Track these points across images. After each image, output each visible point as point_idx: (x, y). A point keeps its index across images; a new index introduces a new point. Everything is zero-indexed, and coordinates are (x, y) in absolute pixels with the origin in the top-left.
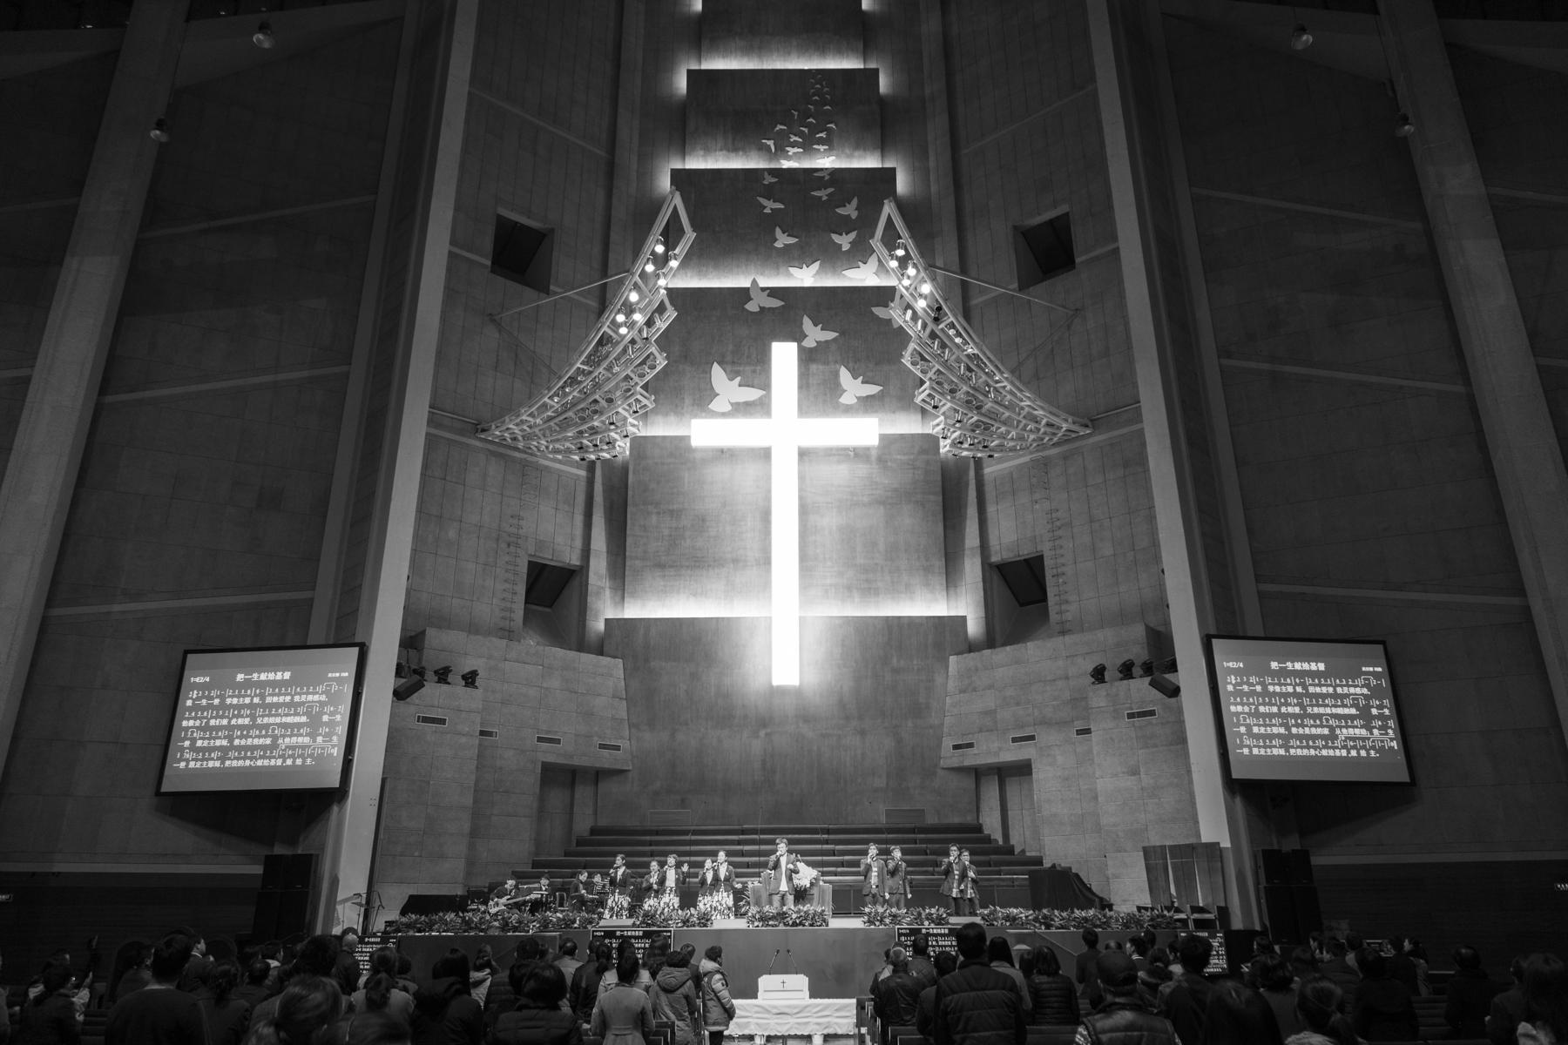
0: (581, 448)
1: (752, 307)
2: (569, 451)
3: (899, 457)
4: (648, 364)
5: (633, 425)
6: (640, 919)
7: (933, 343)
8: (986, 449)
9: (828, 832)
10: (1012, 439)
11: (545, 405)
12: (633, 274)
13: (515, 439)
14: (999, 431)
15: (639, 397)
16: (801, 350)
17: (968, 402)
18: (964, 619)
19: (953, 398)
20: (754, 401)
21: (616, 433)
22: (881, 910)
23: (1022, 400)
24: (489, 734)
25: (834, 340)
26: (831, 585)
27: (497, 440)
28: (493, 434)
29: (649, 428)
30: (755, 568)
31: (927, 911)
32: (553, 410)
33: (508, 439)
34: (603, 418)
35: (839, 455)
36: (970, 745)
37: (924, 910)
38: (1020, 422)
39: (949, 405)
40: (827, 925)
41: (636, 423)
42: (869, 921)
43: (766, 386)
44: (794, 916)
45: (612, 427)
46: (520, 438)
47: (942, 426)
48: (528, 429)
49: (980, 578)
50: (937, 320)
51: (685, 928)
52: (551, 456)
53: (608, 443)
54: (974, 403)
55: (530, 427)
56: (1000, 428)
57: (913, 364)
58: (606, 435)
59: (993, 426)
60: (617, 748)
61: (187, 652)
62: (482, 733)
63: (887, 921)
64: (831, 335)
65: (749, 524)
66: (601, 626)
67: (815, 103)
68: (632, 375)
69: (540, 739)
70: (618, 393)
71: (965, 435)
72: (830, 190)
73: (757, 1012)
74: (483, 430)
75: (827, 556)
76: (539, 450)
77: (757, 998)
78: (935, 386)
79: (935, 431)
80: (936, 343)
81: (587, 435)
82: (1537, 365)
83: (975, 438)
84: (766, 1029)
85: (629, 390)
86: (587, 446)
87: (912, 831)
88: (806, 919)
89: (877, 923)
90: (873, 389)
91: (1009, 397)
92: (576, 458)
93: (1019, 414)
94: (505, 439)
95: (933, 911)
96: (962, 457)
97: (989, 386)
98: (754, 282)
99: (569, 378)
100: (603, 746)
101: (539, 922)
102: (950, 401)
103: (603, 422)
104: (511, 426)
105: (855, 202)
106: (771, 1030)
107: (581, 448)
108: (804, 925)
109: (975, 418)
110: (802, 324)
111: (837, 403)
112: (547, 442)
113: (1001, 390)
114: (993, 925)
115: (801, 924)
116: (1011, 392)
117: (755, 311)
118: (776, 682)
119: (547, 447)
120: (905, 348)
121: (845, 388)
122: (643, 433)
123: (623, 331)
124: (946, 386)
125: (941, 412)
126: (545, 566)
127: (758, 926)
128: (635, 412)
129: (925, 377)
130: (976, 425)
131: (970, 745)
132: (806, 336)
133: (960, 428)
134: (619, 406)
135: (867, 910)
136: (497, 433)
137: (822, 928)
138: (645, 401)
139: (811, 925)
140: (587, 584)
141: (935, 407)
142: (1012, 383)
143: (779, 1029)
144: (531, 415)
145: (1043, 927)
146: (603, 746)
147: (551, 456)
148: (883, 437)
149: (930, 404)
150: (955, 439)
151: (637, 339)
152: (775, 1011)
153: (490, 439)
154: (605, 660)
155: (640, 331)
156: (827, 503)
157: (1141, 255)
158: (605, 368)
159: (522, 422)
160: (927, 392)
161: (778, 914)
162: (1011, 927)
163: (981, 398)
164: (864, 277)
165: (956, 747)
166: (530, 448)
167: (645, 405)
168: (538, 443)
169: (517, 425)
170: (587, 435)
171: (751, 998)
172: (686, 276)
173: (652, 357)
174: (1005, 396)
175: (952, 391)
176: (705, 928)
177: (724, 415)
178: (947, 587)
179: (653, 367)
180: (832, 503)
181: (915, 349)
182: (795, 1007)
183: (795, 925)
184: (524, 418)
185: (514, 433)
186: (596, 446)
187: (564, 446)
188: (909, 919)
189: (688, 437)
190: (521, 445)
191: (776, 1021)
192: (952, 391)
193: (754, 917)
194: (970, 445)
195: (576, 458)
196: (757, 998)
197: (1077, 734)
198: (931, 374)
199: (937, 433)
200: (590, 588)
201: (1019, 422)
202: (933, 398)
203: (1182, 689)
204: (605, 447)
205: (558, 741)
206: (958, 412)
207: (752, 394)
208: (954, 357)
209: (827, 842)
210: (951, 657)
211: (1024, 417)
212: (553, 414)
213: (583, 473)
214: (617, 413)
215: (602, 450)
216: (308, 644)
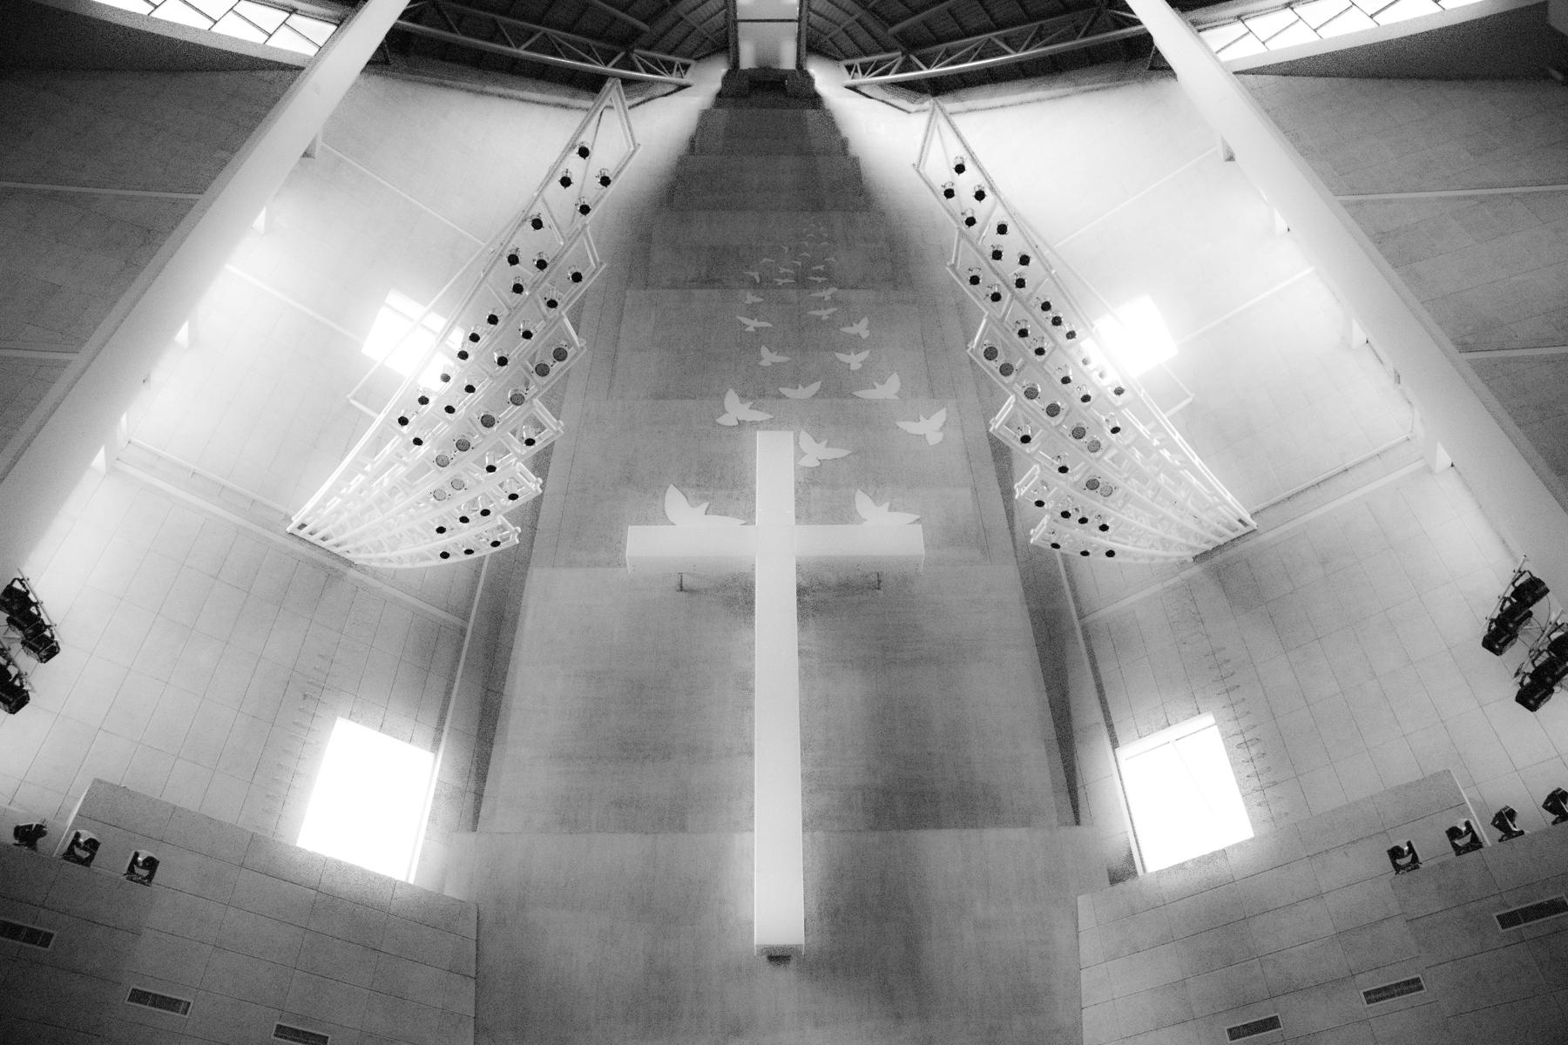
64: (840, 453)
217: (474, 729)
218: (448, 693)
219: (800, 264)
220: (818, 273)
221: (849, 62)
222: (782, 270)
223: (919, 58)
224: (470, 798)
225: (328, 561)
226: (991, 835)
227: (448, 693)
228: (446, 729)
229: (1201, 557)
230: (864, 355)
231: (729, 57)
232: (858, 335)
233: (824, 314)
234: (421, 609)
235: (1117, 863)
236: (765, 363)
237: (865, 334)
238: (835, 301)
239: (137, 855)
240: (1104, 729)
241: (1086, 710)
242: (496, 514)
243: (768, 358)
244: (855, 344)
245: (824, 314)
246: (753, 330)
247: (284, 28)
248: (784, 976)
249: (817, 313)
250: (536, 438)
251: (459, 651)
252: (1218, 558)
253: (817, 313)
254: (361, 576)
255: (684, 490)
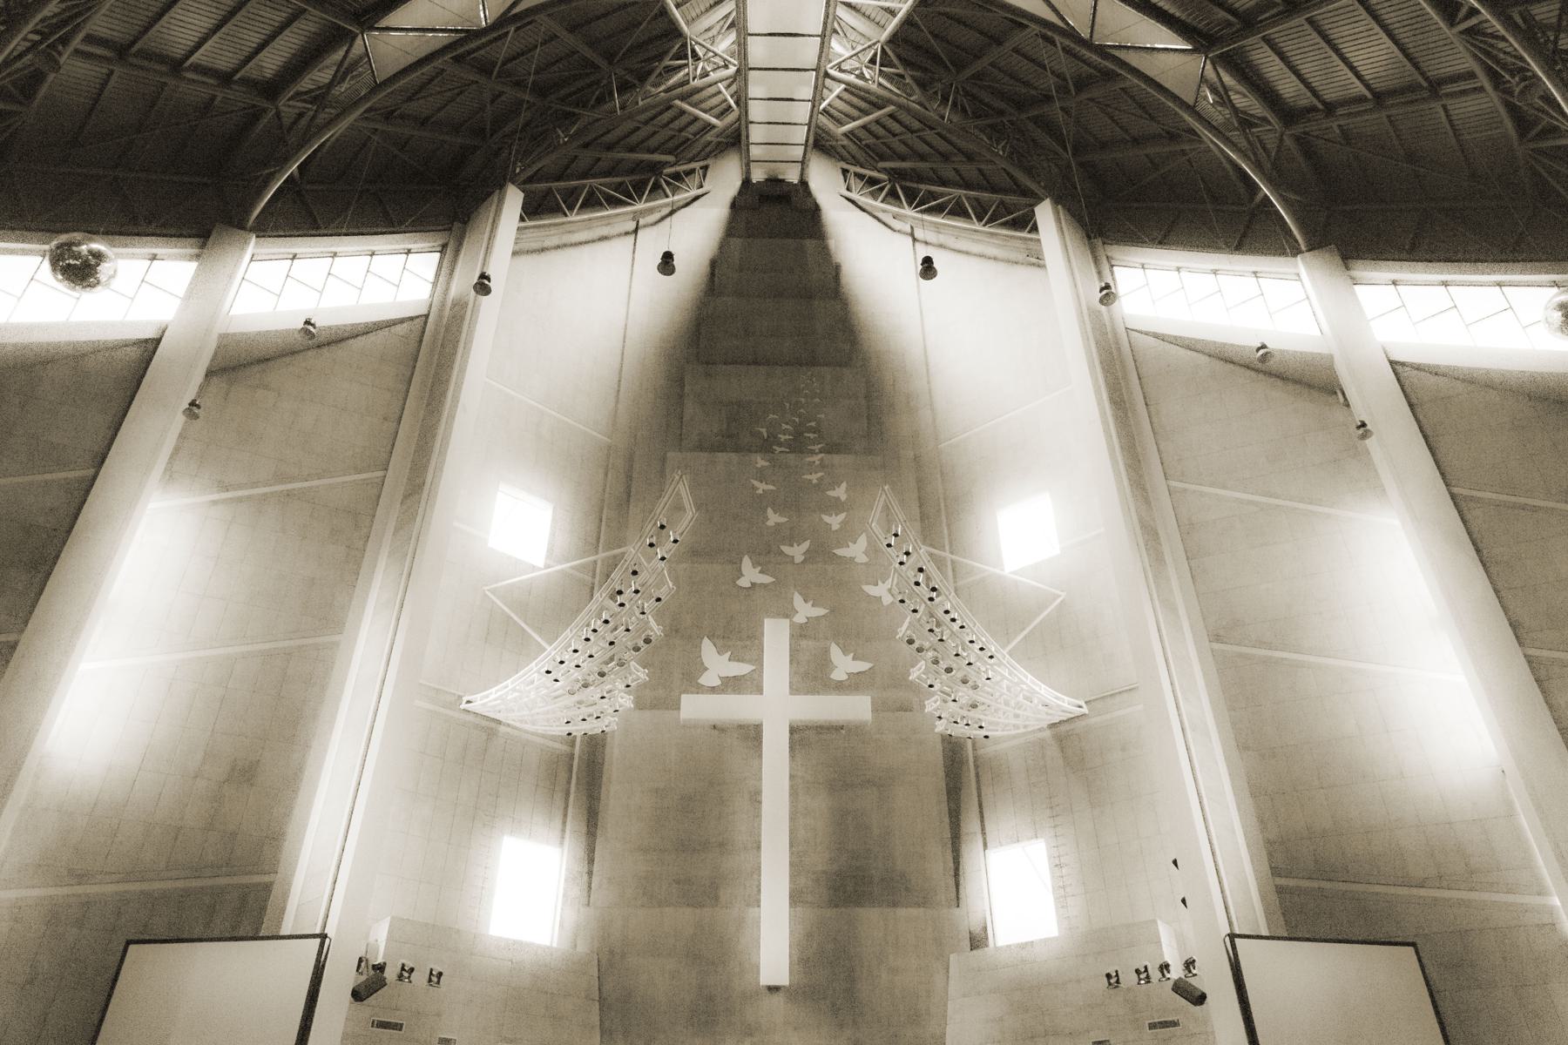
16: (792, 625)
43: (759, 661)
61: (129, 943)
64: (820, 612)
67: (806, 396)
72: (820, 474)
82: (1525, 656)
105: (844, 485)
157: (1254, 1015)
177: (713, 690)
197: (402, 1025)
203: (490, 295)
207: (742, 669)
216: (282, 933)
217: (584, 829)
218: (566, 808)
219: (797, 420)
220: (811, 430)
221: (846, 166)
222: (784, 426)
223: (902, 188)
224: (586, 877)
225: (485, 723)
226: (902, 912)
227: (566, 808)
228: (568, 832)
229: (1052, 726)
230: (842, 516)
231: (741, 154)
232: (838, 498)
233: (814, 478)
234: (548, 747)
235: (977, 930)
236: (770, 523)
237: (843, 497)
238: (823, 466)
239: (432, 970)
240: (979, 837)
241: (970, 824)
242: (581, 654)
243: (773, 518)
244: (836, 506)
245: (814, 478)
246: (762, 492)
247: (426, 313)
248: (778, 1000)
249: (809, 477)
250: (610, 620)
251: (570, 778)
252: (1063, 728)
253: (809, 477)
254: (509, 730)
255: (715, 640)
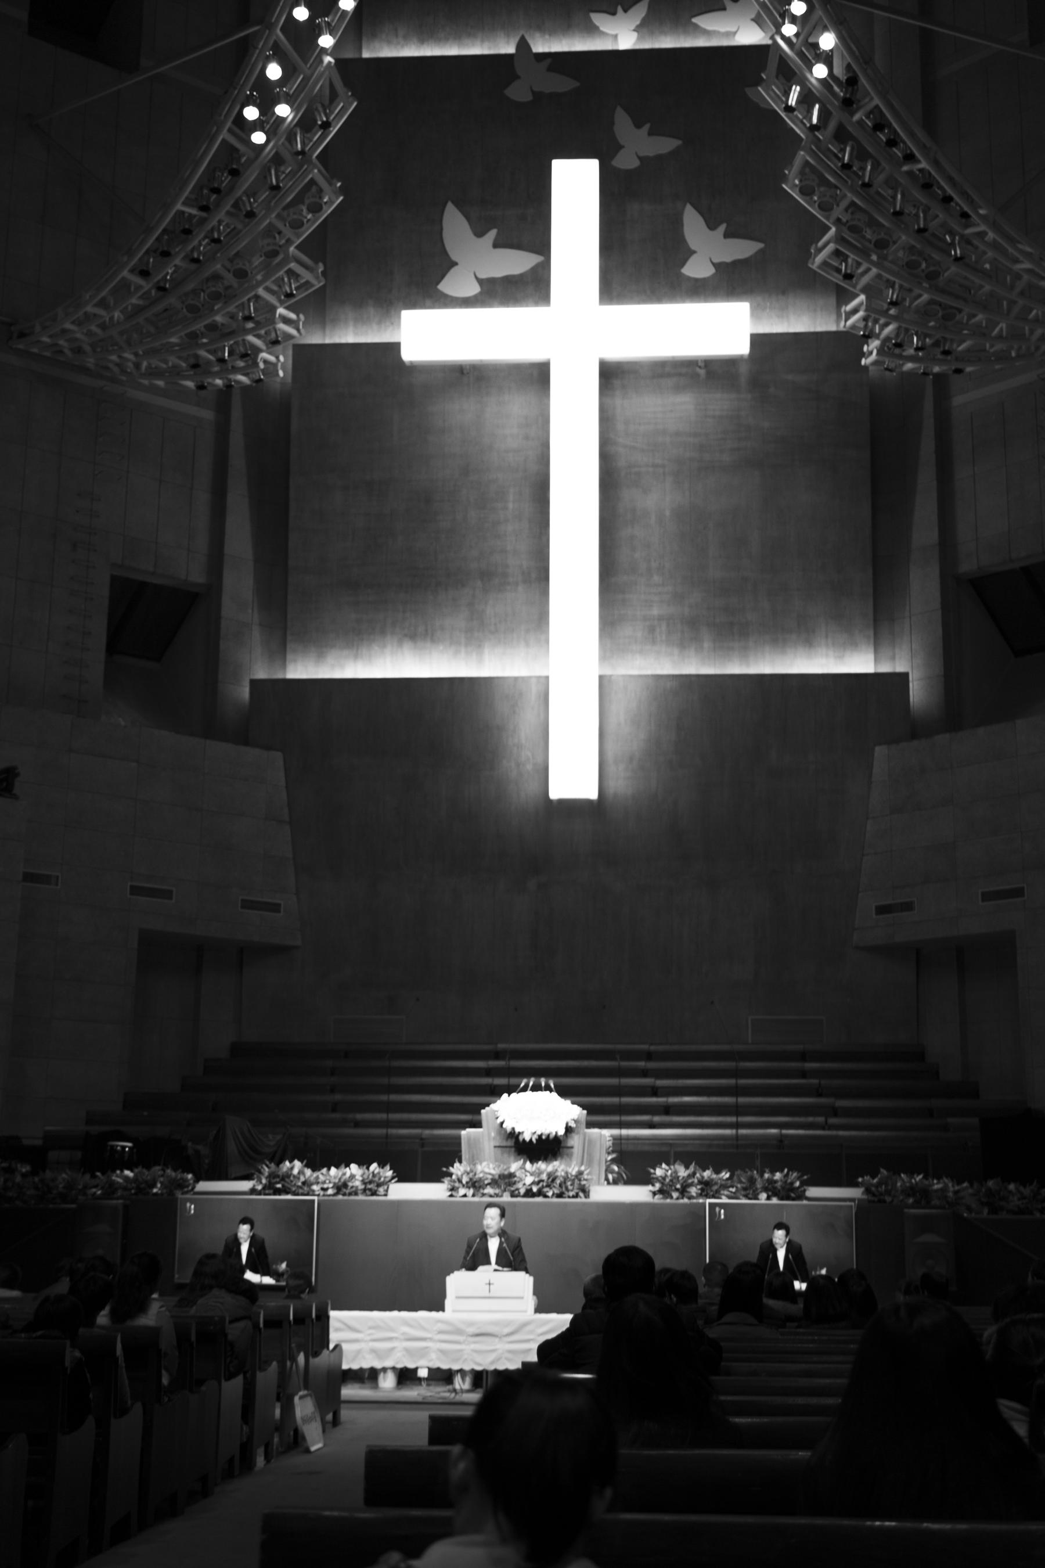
0: (195, 366)
1: (518, 92)
2: (176, 372)
3: (790, 377)
4: (307, 202)
5: (286, 321)
6: (264, 1181)
7: (843, 151)
8: (949, 358)
9: (649, 1056)
10: (1000, 337)
11: (125, 285)
12: (271, 27)
13: (78, 351)
14: (973, 321)
15: (293, 265)
17: (911, 265)
18: (905, 675)
19: (883, 258)
20: (521, 276)
21: (258, 336)
22: (682, 1172)
23: (1016, 261)
24: (45, 879)
25: (674, 153)
26: (660, 618)
27: (47, 354)
28: (39, 341)
29: (328, 332)
30: (520, 588)
31: (766, 1176)
32: (140, 294)
33: (67, 351)
34: (231, 308)
35: (680, 375)
36: (908, 907)
37: (762, 1176)
38: (1015, 302)
39: (874, 271)
40: (586, 1193)
41: (293, 316)
42: (661, 1191)
43: (541, 245)
44: (529, 1180)
45: (250, 325)
46: (87, 348)
47: (861, 314)
48: (98, 331)
49: (936, 603)
50: (848, 103)
51: (340, 1197)
52: (146, 382)
53: (244, 356)
54: (924, 265)
55: (103, 327)
56: (974, 316)
57: (805, 191)
58: (240, 339)
59: (960, 311)
60: (275, 908)
62: (28, 877)
63: (694, 1191)
64: (666, 145)
65: (511, 506)
66: (245, 692)
68: (280, 225)
69: (135, 890)
70: (257, 261)
71: (907, 330)
73: (441, 1332)
74: (22, 335)
75: (654, 565)
76: (123, 371)
77: (443, 1310)
78: (847, 235)
79: (850, 322)
80: (848, 149)
81: (205, 340)
83: (926, 336)
84: (456, 1360)
85: (274, 254)
86: (209, 362)
87: (803, 1057)
88: (548, 1186)
89: (675, 1195)
90: (744, 249)
91: (990, 254)
92: (190, 384)
93: (1012, 287)
94: (61, 352)
95: (778, 1176)
96: (903, 373)
97: (952, 234)
98: (523, 45)
99: (165, 231)
100: (248, 905)
101: (102, 1188)
102: (876, 265)
103: (233, 317)
104: (68, 326)
106: (465, 1360)
107: (195, 366)
108: (546, 1196)
109: (926, 297)
110: (613, 123)
111: (680, 276)
112: (136, 354)
113: (975, 242)
114: (885, 1202)
115: (540, 1193)
116: (995, 245)
117: (525, 100)
118: (556, 792)
119: (137, 366)
120: (790, 163)
121: (693, 247)
122: (315, 338)
123: (258, 138)
124: (868, 234)
125: (860, 286)
126: (143, 585)
127: (465, 1196)
128: (290, 295)
129: (828, 218)
130: (925, 312)
131: (908, 907)
132: (621, 147)
133: (895, 318)
134: (259, 284)
135: (659, 1172)
136: (46, 339)
137: (578, 1200)
138: (306, 275)
139: (560, 1195)
140: (218, 618)
141: (848, 277)
142: (995, 226)
143: (479, 1359)
144: (103, 304)
145: (986, 1211)
146: (248, 905)
147: (146, 382)
148: (756, 340)
149: (839, 271)
150: (887, 339)
151: (287, 156)
152: (472, 1330)
153: (35, 350)
154: (251, 754)
155: (291, 137)
156: (655, 466)
158: (228, 213)
159: (88, 318)
160: (831, 247)
161: (502, 1177)
162: (917, 1205)
163: (936, 256)
164: (734, 30)
165: (882, 910)
166: (107, 368)
167: (307, 283)
168: (120, 357)
169: (79, 323)
170: (205, 340)
171: (438, 1310)
172: (397, 36)
173: (314, 189)
174: (985, 253)
175: (881, 245)
176: (374, 1198)
178: (875, 620)
179: (316, 209)
180: (663, 466)
181: (807, 163)
182: (508, 1323)
183: (529, 1193)
184: (89, 309)
185: (77, 339)
186: (222, 360)
187: (166, 362)
188: (733, 1190)
189: (395, 347)
190: (90, 362)
191: (473, 1346)
192: (881, 245)
193: (460, 1181)
194: (918, 349)
195: (190, 384)
196: (443, 1310)
198: (838, 212)
199: (853, 327)
200: (223, 624)
201: (1012, 303)
202: (845, 259)
204: (241, 364)
205: (167, 894)
206: (893, 287)
208: (882, 177)
209: (645, 1073)
210: (877, 749)
211: (1022, 293)
212: (141, 302)
213: (208, 415)
214: (257, 297)
215: (235, 370)
